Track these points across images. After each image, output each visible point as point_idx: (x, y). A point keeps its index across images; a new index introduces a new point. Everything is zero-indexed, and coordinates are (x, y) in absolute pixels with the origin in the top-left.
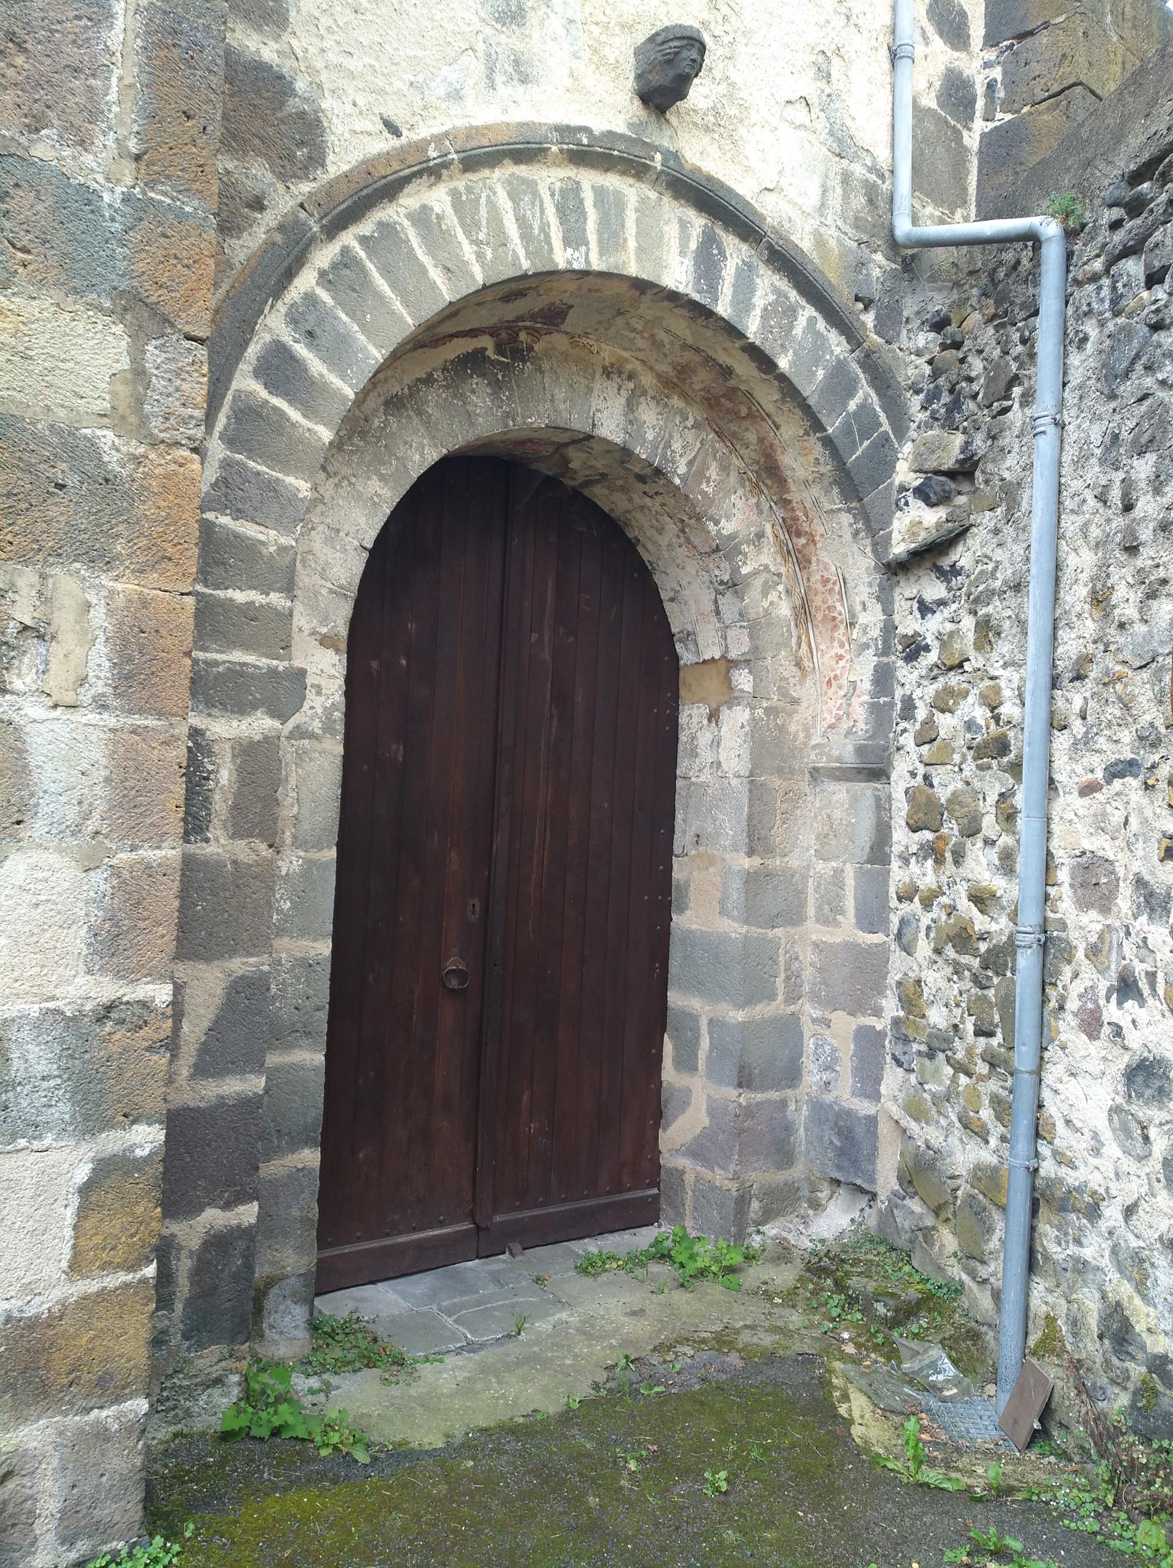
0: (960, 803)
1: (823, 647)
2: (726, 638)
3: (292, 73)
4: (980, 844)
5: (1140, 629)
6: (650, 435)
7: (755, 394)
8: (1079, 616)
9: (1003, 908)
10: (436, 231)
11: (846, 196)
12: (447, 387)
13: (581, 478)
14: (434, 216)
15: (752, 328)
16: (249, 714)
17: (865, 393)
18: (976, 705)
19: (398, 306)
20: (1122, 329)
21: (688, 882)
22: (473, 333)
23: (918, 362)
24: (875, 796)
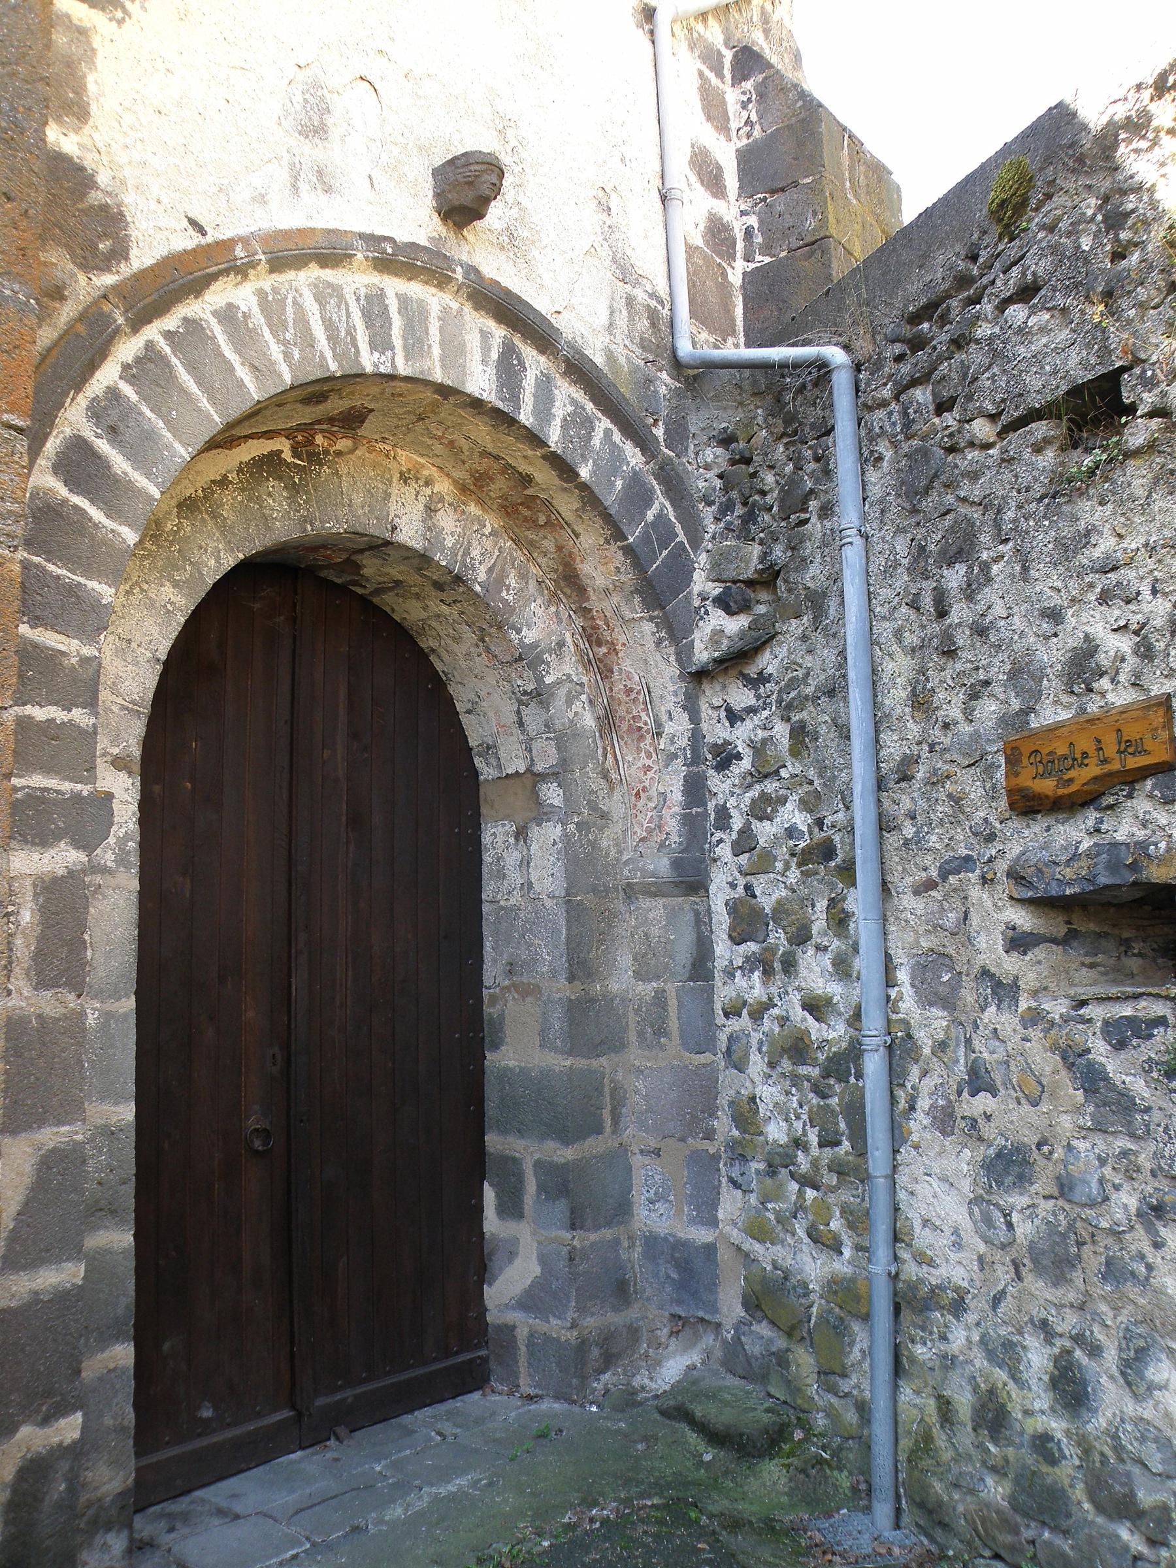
0: (787, 912)
1: (629, 758)
2: (530, 751)
3: (94, 166)
4: (811, 952)
5: (965, 728)
6: (449, 542)
7: (555, 502)
8: (899, 719)
9: (840, 1014)
10: (242, 330)
11: (631, 317)
12: (243, 490)
13: (370, 587)
14: (240, 315)
15: (554, 436)
16: (51, 846)
17: (661, 503)
18: (796, 812)
19: (204, 403)
20: (918, 450)
21: (502, 1016)
22: (269, 435)
23: (708, 476)
24: (693, 910)
